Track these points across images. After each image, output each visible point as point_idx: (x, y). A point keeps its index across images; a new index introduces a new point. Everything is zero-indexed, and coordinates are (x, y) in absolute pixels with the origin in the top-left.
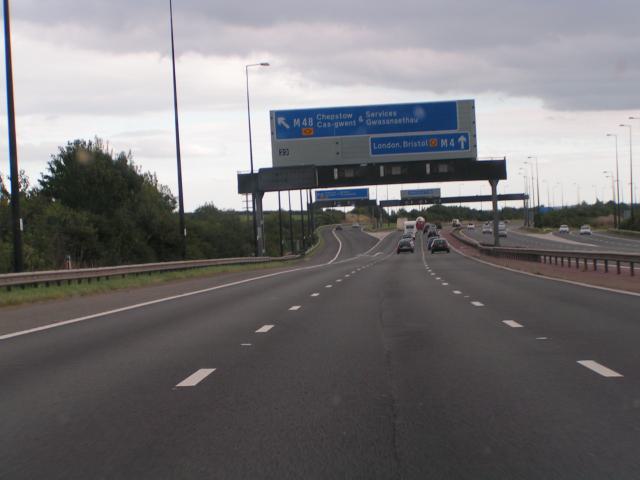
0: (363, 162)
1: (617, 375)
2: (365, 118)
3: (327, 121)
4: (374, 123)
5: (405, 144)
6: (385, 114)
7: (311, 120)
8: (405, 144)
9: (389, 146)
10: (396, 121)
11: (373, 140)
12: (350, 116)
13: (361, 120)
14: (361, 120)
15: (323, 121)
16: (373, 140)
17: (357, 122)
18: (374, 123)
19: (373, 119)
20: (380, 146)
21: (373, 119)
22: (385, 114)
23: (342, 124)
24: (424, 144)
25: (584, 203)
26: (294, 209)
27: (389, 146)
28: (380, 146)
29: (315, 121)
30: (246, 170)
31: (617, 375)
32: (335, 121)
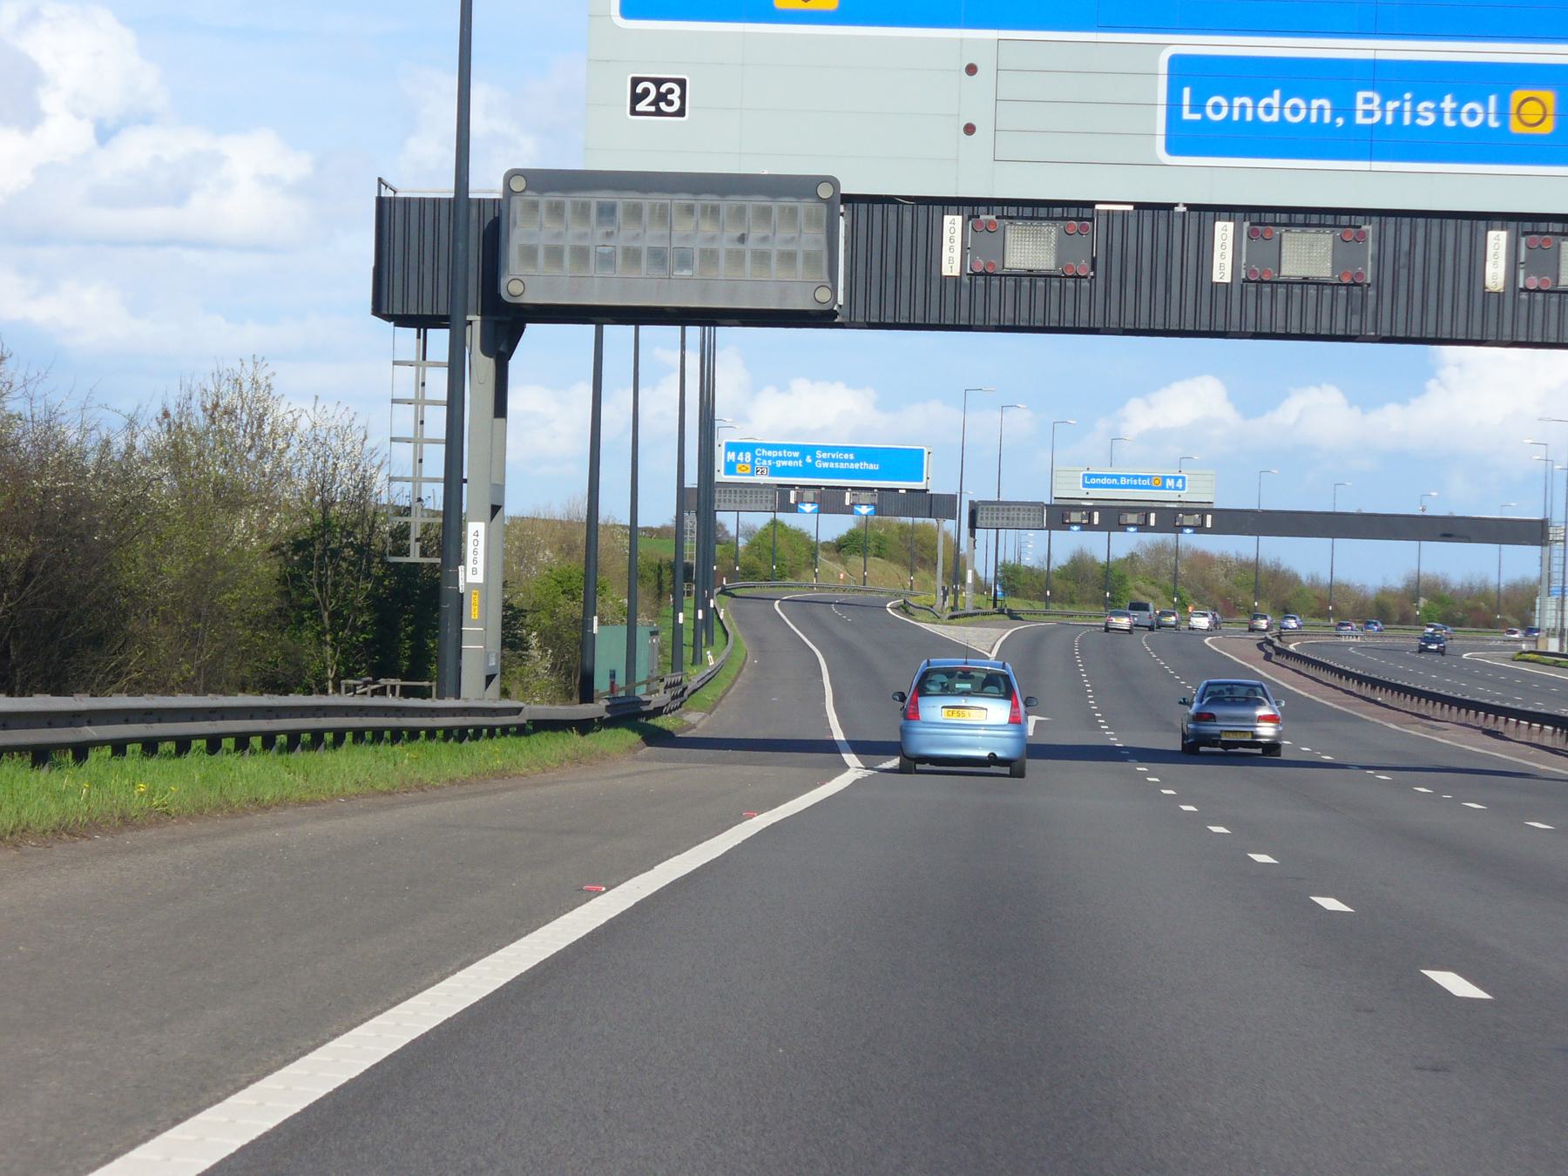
0: (1114, 187)
1: (1434, 975)
2: (814, 459)
3: (768, 458)
4: (826, 465)
5: (1368, 107)
6: (839, 456)
7: (748, 455)
8: (1368, 107)
9: (1274, 108)
10: (852, 466)
11: (1182, 70)
12: (796, 454)
13: (809, 459)
14: (809, 459)
15: (763, 458)
16: (1182, 70)
17: (804, 462)
18: (826, 465)
19: (824, 460)
20: (1219, 108)
21: (824, 460)
22: (839, 456)
23: (784, 463)
24: (1479, 114)
25: (1278, 565)
26: (697, 329)
27: (1274, 108)
28: (1219, 108)
29: (754, 457)
30: (425, 174)
31: (1434, 975)
32: (778, 458)
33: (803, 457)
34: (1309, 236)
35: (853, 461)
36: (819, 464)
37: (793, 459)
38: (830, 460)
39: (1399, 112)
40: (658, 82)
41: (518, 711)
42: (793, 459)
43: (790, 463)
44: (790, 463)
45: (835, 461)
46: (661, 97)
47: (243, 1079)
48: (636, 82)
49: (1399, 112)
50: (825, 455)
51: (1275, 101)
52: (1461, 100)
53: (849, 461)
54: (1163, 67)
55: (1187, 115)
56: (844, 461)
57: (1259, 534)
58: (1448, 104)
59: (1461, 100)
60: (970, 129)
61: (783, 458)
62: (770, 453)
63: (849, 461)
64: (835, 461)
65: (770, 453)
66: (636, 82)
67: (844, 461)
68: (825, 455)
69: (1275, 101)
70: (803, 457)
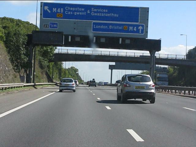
1: (128, 100)
2: (91, 12)
3: (70, 11)
4: (96, 14)
7: (62, 9)
12: (83, 9)
18: (96, 14)
19: (95, 12)
21: (95, 12)
24: (120, 28)
28: (97, 27)
29: (64, 10)
31: (128, 100)
32: (75, 11)
33: (86, 11)
34: (103, 38)
35: (108, 13)
36: (93, 14)
37: (81, 11)
38: (97, 12)
39: (113, 28)
40: (46, 25)
41: (23, 84)
42: (81, 11)
43: (81, 13)
44: (81, 13)
45: (100, 12)
46: (47, 26)
47: (78, 46)
48: (44, 25)
49: (113, 28)
50: (95, 10)
51: (102, 26)
52: (119, 27)
53: (106, 13)
54: (92, 23)
55: (94, 27)
56: (104, 13)
57: (143, 56)
58: (118, 27)
59: (119, 27)
60: (75, 29)
61: (77, 11)
62: (71, 9)
63: (106, 13)
64: (100, 12)
65: (71, 9)
66: (44, 25)
67: (104, 13)
68: (95, 10)
69: (102, 26)
70: (86, 11)
